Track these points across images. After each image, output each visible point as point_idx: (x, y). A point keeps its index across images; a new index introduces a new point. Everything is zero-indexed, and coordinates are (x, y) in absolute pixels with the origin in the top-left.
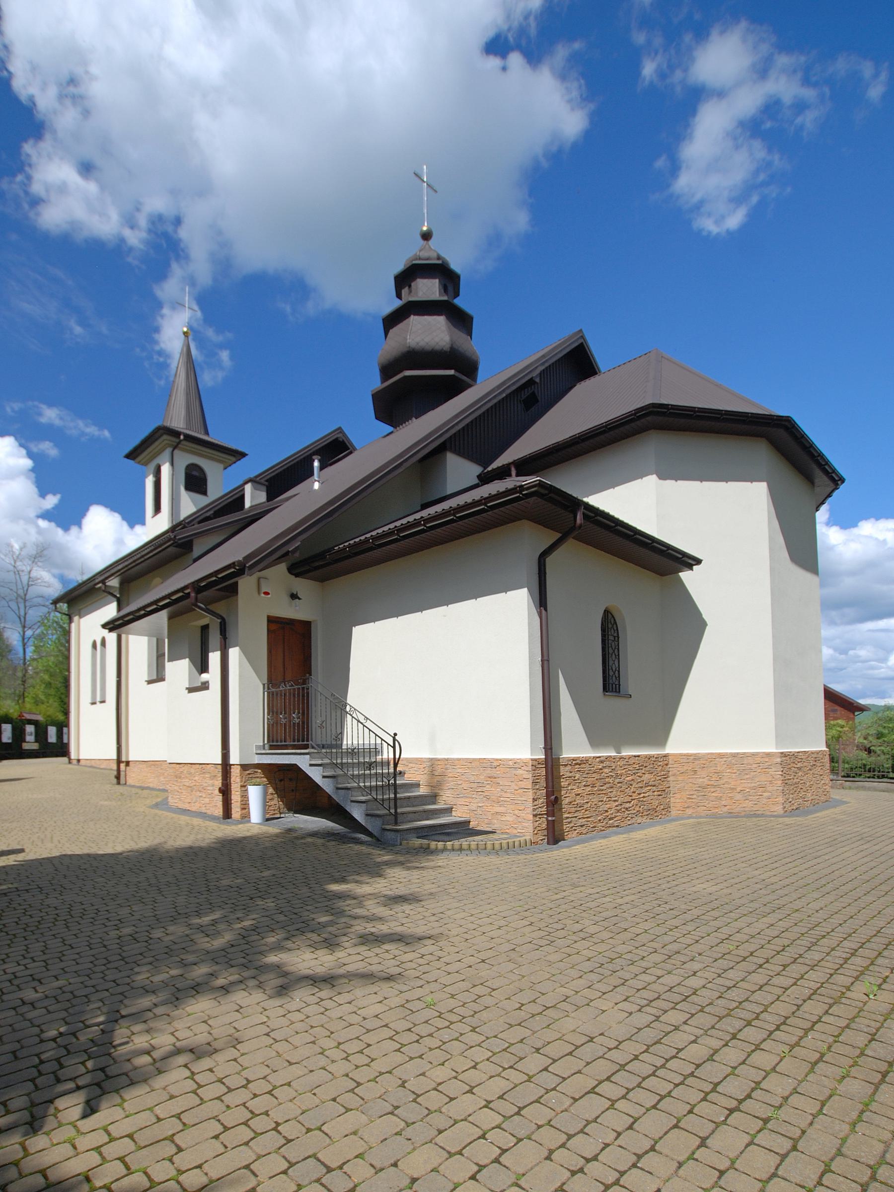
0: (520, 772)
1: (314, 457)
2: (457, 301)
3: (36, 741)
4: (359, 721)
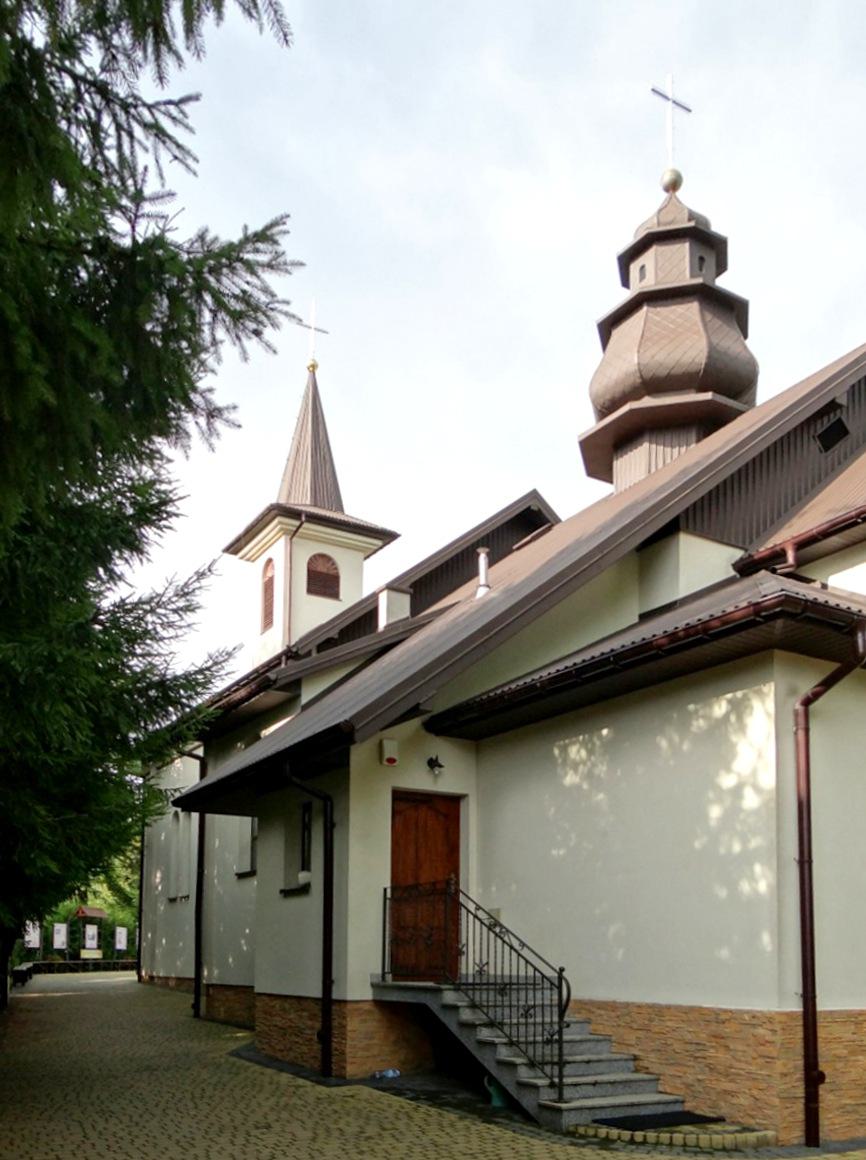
0: (761, 1031)
1: (480, 550)
2: (723, 282)
3: (99, 947)
4: (512, 947)
